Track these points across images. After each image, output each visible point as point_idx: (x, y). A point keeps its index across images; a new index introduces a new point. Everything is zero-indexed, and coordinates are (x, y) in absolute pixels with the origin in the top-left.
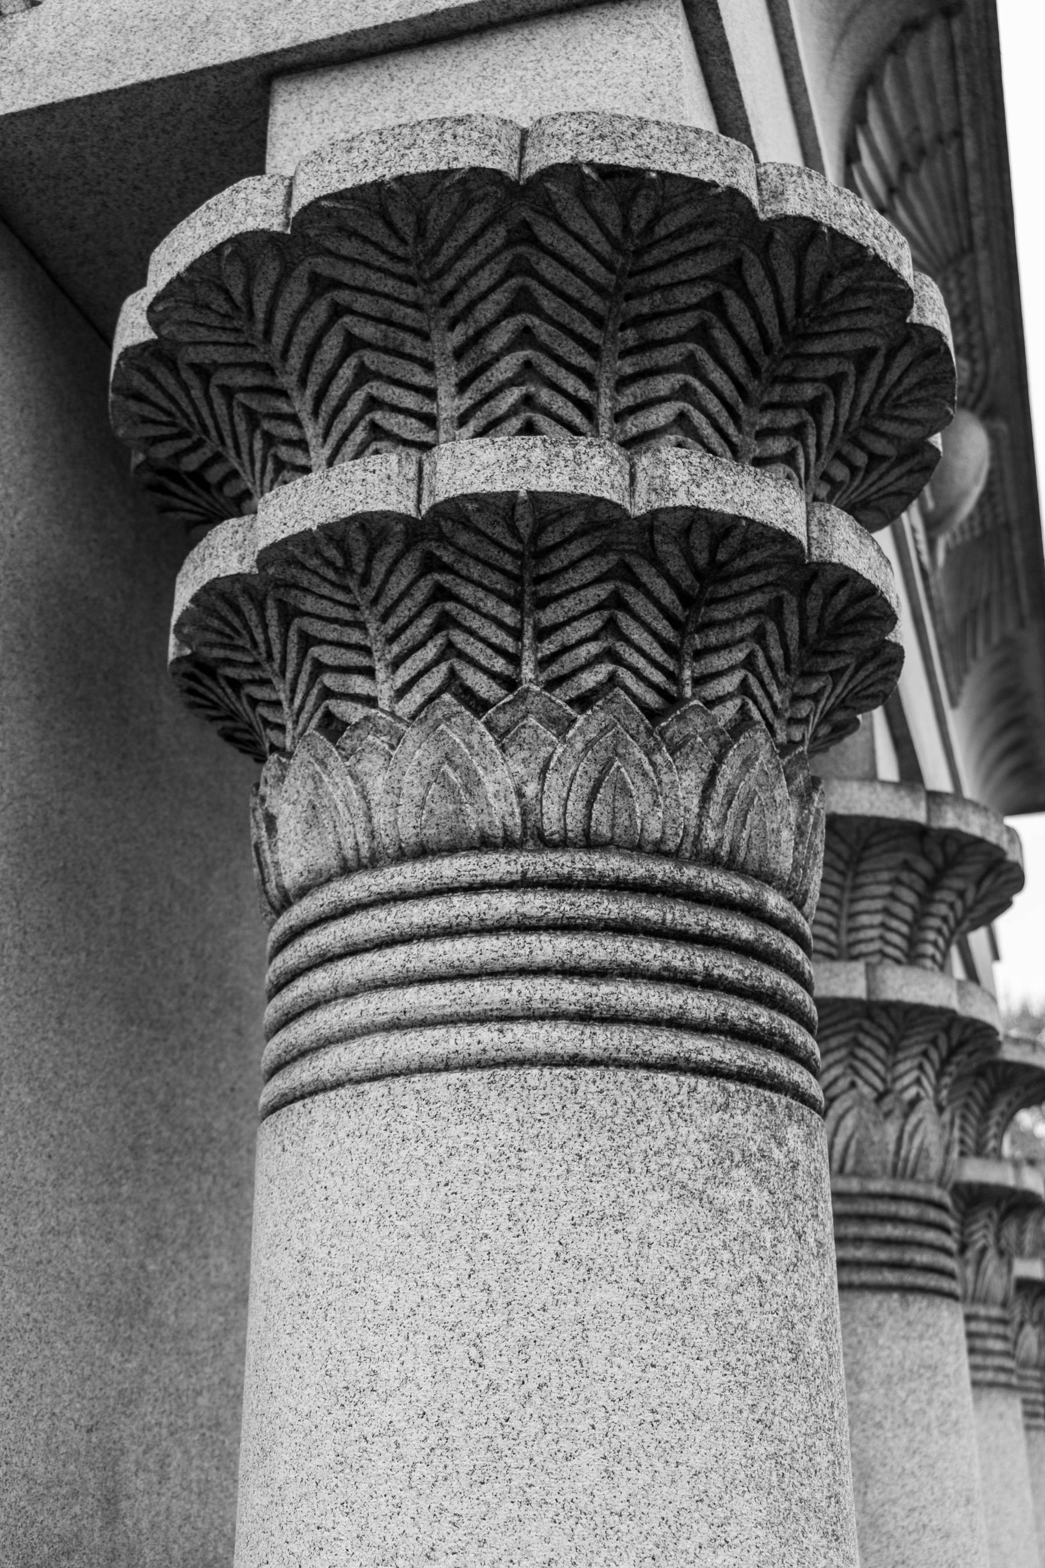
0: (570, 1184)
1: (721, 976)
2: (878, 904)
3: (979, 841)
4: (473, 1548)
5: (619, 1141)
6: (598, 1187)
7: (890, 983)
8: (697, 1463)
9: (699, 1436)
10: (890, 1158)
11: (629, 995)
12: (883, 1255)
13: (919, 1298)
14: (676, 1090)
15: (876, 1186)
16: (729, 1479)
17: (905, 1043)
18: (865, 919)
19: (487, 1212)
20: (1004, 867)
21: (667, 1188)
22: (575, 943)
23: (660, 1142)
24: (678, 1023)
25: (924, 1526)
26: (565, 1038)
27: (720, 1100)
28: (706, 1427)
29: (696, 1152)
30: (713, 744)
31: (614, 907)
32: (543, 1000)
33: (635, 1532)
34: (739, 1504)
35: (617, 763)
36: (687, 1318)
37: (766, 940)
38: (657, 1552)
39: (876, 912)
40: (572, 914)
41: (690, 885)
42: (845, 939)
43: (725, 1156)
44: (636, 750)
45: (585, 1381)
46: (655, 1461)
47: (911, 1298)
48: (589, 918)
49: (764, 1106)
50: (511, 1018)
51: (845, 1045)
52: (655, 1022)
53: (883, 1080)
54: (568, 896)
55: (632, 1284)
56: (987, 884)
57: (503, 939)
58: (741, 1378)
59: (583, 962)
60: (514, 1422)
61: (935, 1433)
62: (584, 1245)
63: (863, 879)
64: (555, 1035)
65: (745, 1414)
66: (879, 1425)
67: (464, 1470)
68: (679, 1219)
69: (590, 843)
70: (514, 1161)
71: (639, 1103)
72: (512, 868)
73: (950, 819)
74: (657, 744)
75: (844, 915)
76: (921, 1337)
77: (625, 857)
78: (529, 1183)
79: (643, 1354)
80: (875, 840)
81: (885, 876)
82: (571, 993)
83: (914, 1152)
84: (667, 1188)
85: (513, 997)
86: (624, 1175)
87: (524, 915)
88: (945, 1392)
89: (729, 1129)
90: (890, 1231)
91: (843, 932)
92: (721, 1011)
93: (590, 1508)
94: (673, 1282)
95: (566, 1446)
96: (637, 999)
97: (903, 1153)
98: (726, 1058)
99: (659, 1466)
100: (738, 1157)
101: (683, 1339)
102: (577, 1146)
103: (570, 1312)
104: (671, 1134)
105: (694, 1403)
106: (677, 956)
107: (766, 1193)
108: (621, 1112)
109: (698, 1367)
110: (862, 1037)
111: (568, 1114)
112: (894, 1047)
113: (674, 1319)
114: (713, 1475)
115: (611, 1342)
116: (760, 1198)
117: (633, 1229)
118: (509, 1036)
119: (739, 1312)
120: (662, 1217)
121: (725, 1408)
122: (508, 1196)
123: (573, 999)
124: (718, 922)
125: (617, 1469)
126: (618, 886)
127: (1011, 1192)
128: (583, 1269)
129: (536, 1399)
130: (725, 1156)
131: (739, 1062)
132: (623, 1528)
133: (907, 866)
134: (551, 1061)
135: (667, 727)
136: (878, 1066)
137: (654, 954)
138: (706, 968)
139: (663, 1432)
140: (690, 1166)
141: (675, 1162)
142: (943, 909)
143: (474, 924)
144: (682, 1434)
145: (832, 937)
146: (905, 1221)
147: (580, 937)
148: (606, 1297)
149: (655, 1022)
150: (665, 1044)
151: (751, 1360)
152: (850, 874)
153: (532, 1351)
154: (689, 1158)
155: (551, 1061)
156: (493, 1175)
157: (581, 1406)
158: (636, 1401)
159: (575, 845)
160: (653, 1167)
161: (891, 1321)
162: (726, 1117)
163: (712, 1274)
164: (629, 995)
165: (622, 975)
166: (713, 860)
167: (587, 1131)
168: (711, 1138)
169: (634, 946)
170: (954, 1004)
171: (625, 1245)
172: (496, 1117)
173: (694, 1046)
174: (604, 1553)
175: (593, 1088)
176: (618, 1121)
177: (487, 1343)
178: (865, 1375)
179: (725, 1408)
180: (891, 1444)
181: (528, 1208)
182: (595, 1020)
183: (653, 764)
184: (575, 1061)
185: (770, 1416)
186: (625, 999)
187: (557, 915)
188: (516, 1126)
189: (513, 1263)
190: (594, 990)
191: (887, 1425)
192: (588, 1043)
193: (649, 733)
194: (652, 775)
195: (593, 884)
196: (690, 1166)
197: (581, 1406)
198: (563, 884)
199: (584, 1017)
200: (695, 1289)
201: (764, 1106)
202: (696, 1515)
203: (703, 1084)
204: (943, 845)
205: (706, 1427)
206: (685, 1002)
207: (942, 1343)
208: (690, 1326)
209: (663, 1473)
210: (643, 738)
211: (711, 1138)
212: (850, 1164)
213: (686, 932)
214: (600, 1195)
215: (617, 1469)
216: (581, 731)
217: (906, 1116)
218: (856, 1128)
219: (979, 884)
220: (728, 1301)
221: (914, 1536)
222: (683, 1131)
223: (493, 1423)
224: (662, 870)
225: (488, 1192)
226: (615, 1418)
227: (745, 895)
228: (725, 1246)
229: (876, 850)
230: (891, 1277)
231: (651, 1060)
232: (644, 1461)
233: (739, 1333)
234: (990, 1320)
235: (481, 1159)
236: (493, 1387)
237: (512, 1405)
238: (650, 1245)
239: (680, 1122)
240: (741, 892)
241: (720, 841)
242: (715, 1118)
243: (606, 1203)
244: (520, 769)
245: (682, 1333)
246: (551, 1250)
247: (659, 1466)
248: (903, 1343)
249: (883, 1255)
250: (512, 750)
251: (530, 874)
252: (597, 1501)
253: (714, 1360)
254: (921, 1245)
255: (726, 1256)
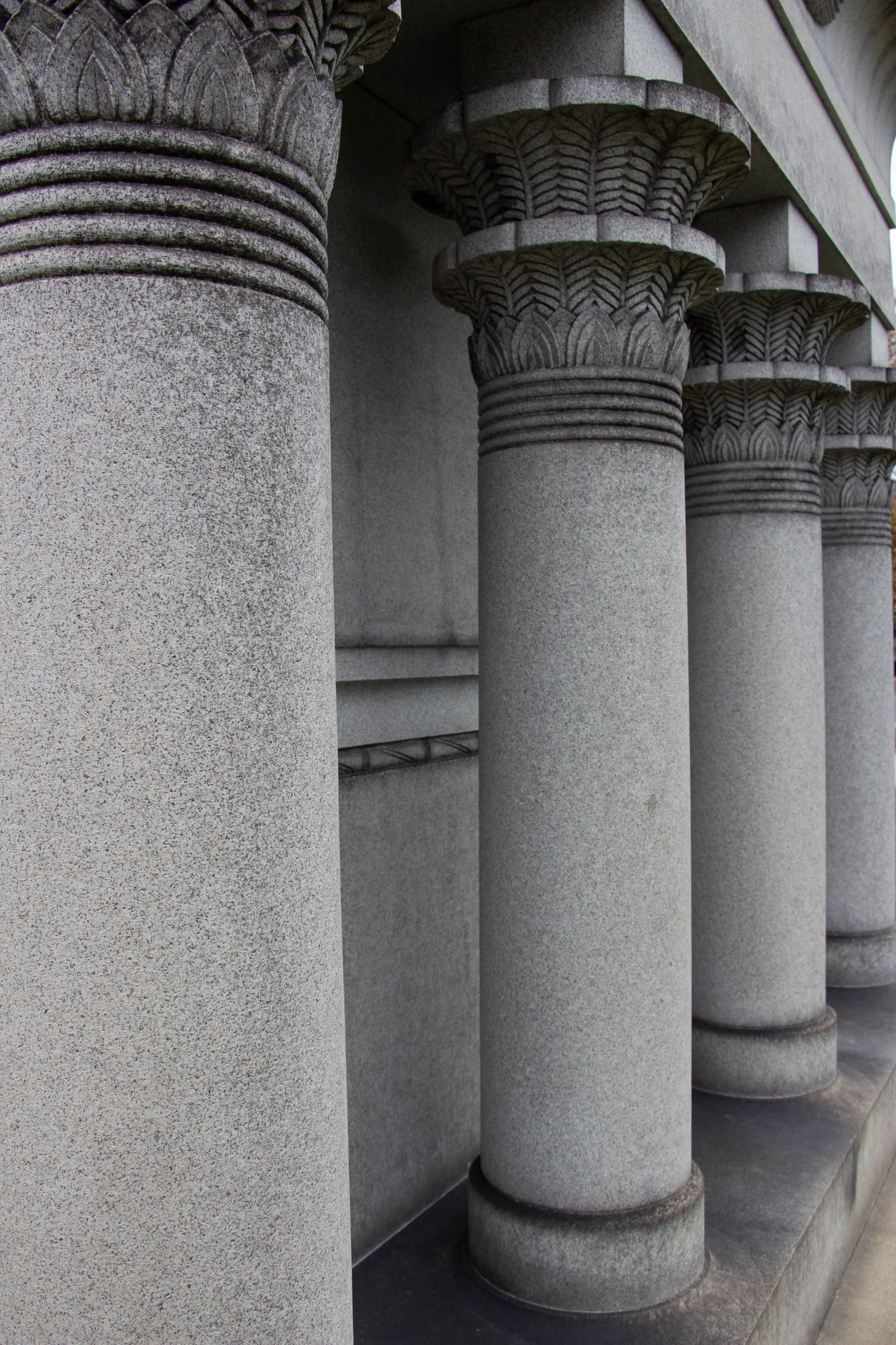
0: (65, 352)
1: (181, 207)
2: (618, 172)
3: (691, 118)
4: (14, 571)
5: (96, 323)
6: (82, 353)
7: (613, 229)
8: (143, 519)
9: (145, 504)
10: (620, 354)
11: (106, 224)
12: (610, 418)
13: (636, 445)
14: (137, 286)
15: (606, 373)
16: (167, 528)
17: (634, 272)
18: (608, 185)
19: (19, 373)
20: (721, 138)
21: (129, 351)
22: (71, 191)
23: (126, 321)
24: (144, 241)
25: (626, 587)
26: (62, 257)
27: (174, 292)
28: (152, 498)
29: (152, 326)
30: (175, 34)
31: (97, 163)
32: (50, 232)
33: (101, 560)
34: (174, 543)
35: (93, 55)
36: (140, 433)
37: (227, 179)
38: (114, 571)
39: (618, 178)
40: (68, 171)
41: (156, 143)
42: (593, 200)
43: (174, 329)
44: (106, 44)
45: (72, 473)
46: (114, 519)
47: (629, 446)
48: (80, 172)
49: (214, 295)
50: (33, 247)
51: (589, 275)
52: (127, 241)
53: (618, 299)
54: (67, 159)
55: (102, 413)
56: (711, 152)
57: (29, 193)
58: (181, 469)
59: (76, 204)
60: (33, 499)
61: (640, 530)
62: (72, 391)
63: (604, 154)
64: (57, 255)
65: (182, 491)
66: (599, 526)
67: (9, 528)
68: (137, 371)
69: (84, 119)
70: (33, 340)
71: (111, 297)
72: (32, 142)
73: (663, 102)
74: (123, 37)
75: (526, 178)
76: (634, 471)
77: (106, 126)
78: (41, 354)
79: (109, 455)
80: (607, 123)
81: (621, 150)
82: (67, 226)
83: (638, 349)
84: (129, 351)
85: (33, 232)
86: (99, 345)
87: (39, 175)
88: (651, 506)
89: (181, 310)
90: (616, 402)
91: (591, 195)
92: (179, 230)
93: (74, 547)
94: (131, 410)
95: (61, 511)
96: (112, 227)
97: (630, 349)
98: (181, 262)
99: (117, 521)
100: (187, 328)
101: (137, 446)
102: (70, 327)
103: (64, 432)
104: (133, 316)
105: (143, 484)
106: (144, 195)
107: (211, 352)
108: (98, 304)
109: (146, 463)
110: (600, 269)
111: (64, 307)
112: (626, 276)
113: (130, 434)
114: (155, 527)
115: (87, 449)
116: (205, 355)
117: (104, 379)
118: (31, 258)
119: (181, 428)
120: (125, 370)
121: (166, 486)
122: (29, 363)
123: (68, 230)
124: (178, 169)
125: (90, 524)
126: (102, 148)
127: (818, 385)
128: (72, 405)
129: (44, 485)
130: (174, 329)
131: (192, 265)
132: (93, 558)
133: (637, 142)
134: (56, 273)
135: (132, 23)
136: (614, 289)
137: (125, 194)
138: (167, 202)
139: (120, 502)
140: (147, 336)
141: (135, 334)
142: (676, 174)
143: (14, 185)
144: (134, 503)
145: (583, 199)
146: (629, 395)
147: (75, 187)
148: (85, 421)
149: (127, 241)
150: (131, 256)
151: (190, 458)
152: (594, 151)
153: (43, 457)
154: (146, 331)
155: (56, 273)
156: (22, 350)
157: (69, 488)
158: (103, 484)
159: (73, 121)
160: (119, 338)
161: (612, 460)
162: (178, 303)
163: (161, 405)
164: (106, 224)
165: (105, 211)
166: (178, 123)
167: (75, 318)
168: (164, 318)
169: (111, 190)
170: (667, 242)
171: (98, 389)
172: (24, 312)
173: (152, 255)
174: (81, 572)
175: (80, 289)
176: (96, 309)
177: (19, 453)
178: (591, 495)
179: (166, 486)
180: (606, 537)
181: (41, 369)
182: (86, 243)
183: (122, 53)
184: (70, 272)
185: (203, 491)
186: (103, 227)
187: (60, 172)
188: (34, 317)
189: (33, 404)
190: (82, 223)
191: (604, 526)
192: (77, 259)
193: (117, 29)
194: (120, 62)
195: (85, 148)
196: (147, 336)
197: (69, 488)
198: (65, 150)
199: (78, 241)
200: (147, 414)
201: (214, 295)
202: (142, 550)
203: (160, 282)
204: (662, 124)
205: (152, 498)
206: (149, 226)
207: (652, 474)
208: (142, 438)
209: (120, 526)
210: (113, 34)
211: (164, 318)
212: (590, 358)
213: (153, 177)
214: (83, 358)
215: (90, 524)
216: (67, 33)
217: (633, 324)
218: (594, 333)
219: (705, 153)
220: (173, 421)
221: (618, 592)
222: (143, 313)
223: (22, 500)
224: (134, 134)
225: (20, 361)
226: (89, 494)
227: (207, 148)
228: (172, 387)
229: (610, 131)
230: (614, 432)
231: (122, 267)
232: (108, 519)
233: (181, 441)
234: (797, 470)
235: (16, 340)
236: (23, 479)
237: (32, 489)
238: (115, 388)
239: (140, 307)
240: (203, 145)
241: (182, 110)
242: (169, 304)
243: (87, 363)
244: (31, 67)
245: (137, 442)
246: (53, 394)
247: (117, 521)
248: (621, 474)
249: (610, 418)
250: (25, 52)
251: (43, 145)
252: (78, 543)
253: (160, 458)
254: (641, 411)
255: (173, 393)
